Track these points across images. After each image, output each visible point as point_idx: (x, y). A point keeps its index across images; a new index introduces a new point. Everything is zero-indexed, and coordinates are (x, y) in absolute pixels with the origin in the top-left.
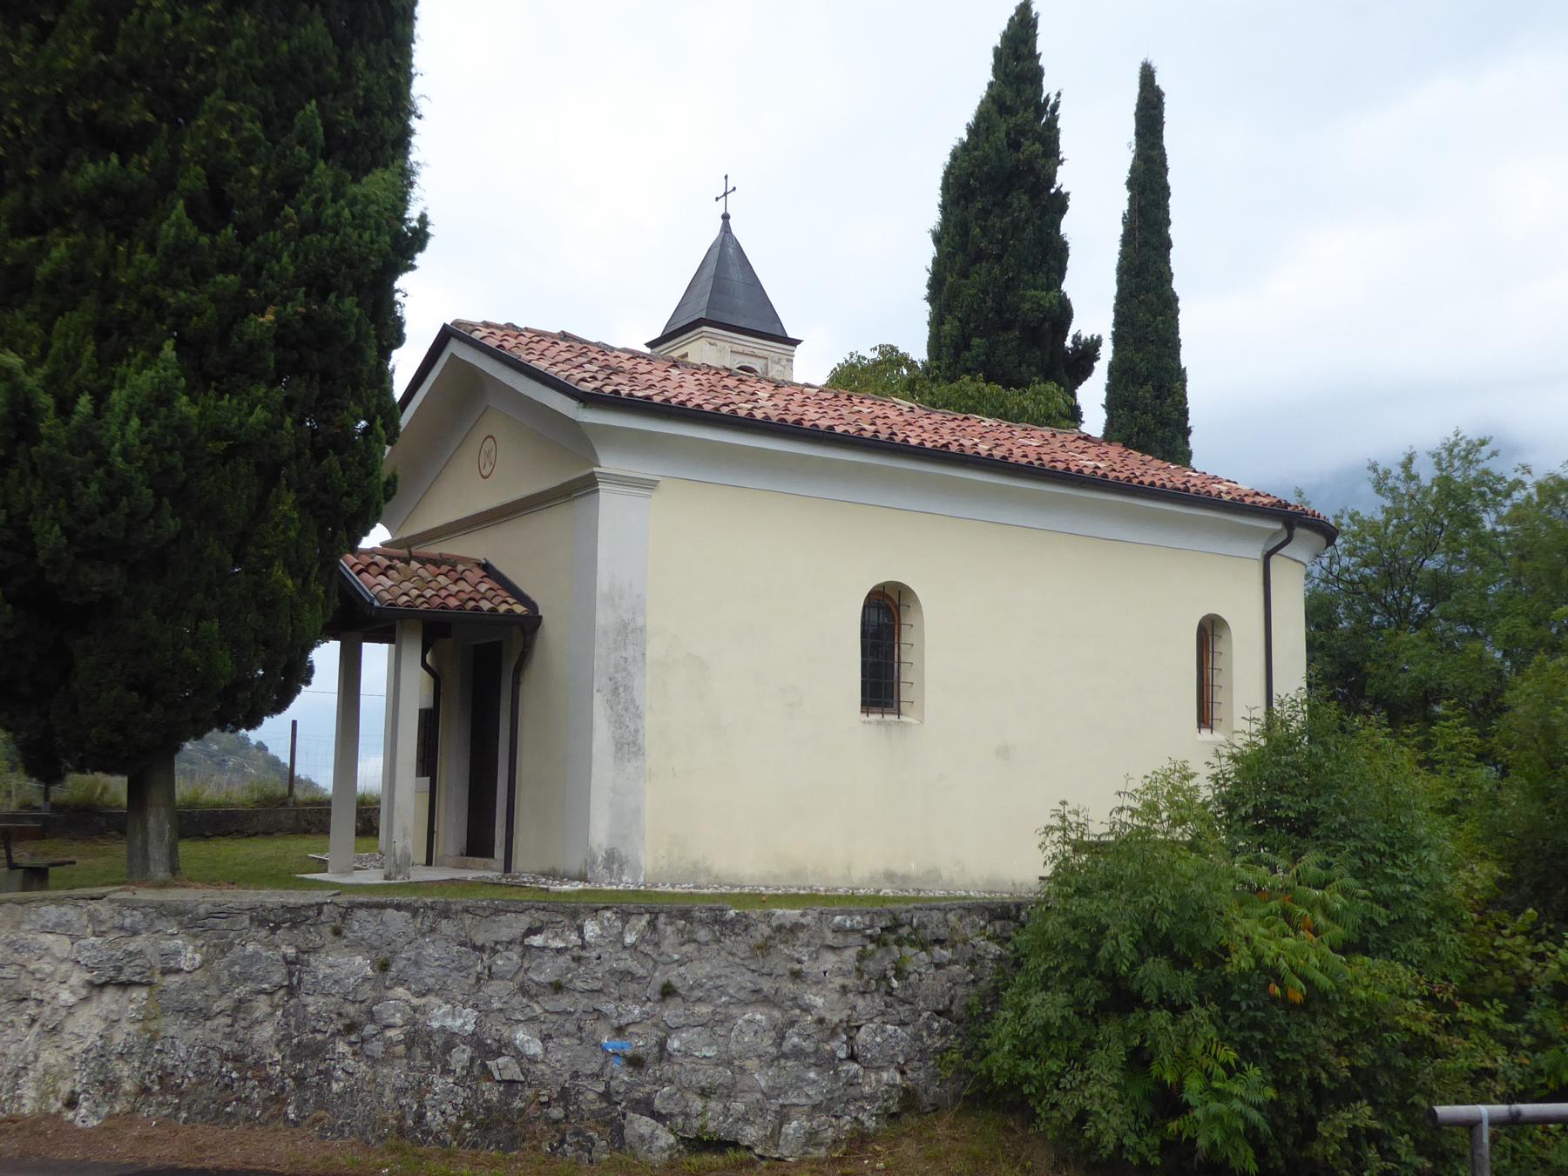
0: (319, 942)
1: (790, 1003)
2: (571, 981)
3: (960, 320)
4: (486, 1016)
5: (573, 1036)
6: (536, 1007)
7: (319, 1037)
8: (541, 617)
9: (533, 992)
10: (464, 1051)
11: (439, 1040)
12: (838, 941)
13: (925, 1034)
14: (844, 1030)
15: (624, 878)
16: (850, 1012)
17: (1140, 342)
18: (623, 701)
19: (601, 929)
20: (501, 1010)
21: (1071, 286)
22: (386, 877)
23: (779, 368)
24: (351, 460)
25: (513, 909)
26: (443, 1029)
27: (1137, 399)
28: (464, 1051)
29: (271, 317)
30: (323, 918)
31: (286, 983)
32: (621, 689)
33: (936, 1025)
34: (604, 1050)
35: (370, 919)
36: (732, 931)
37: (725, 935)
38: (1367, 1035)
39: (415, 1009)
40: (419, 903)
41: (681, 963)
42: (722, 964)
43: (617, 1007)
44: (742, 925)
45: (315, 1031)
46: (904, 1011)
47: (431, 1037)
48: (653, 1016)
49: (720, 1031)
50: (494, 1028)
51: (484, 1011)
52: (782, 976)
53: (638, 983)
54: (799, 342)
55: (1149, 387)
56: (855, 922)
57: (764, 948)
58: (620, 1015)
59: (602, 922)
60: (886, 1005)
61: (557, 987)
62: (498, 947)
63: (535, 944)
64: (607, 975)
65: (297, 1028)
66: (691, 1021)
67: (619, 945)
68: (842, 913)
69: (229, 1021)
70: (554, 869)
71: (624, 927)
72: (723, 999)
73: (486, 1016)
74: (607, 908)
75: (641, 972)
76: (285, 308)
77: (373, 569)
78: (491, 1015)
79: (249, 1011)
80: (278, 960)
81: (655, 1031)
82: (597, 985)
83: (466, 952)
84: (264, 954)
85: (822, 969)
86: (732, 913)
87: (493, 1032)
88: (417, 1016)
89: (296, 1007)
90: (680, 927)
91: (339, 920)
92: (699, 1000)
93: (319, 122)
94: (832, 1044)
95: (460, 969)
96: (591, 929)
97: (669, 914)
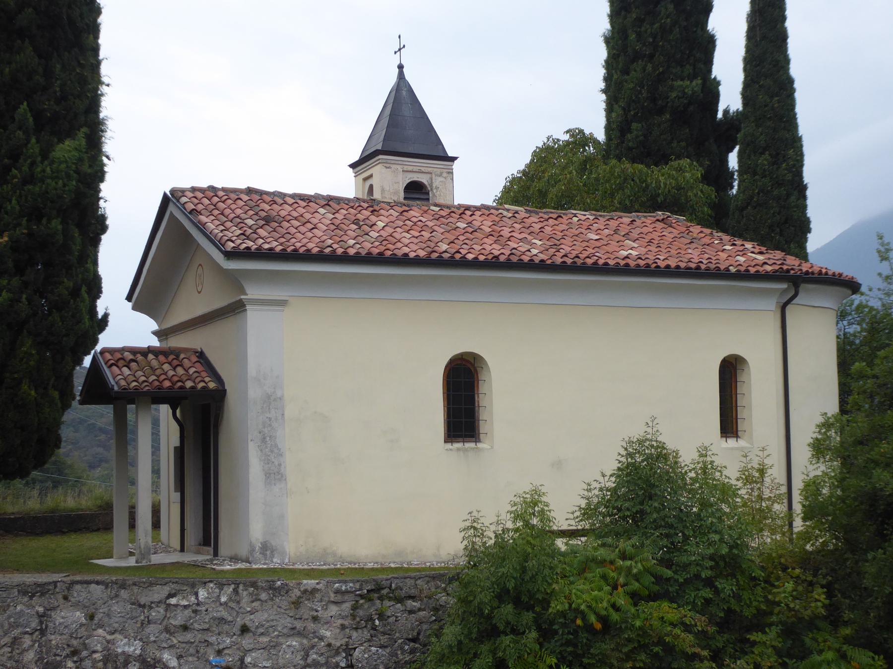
0: (56, 604)
1: (312, 635)
2: (192, 624)
3: (624, 109)
4: (147, 645)
5: (194, 655)
6: (174, 639)
7: (58, 658)
8: (226, 390)
9: (172, 631)
10: (135, 665)
11: (121, 659)
12: (339, 598)
13: (399, 652)
14: (344, 650)
15: (275, 560)
16: (347, 640)
17: (760, 119)
18: (269, 446)
19: (208, 594)
20: (155, 642)
21: (717, 71)
22: (137, 562)
23: (442, 179)
24: (66, 314)
25: (159, 583)
26: (124, 653)
27: (757, 166)
28: (135, 665)
29: (6, 239)
30: (57, 590)
31: (39, 628)
32: (268, 438)
33: (406, 647)
34: (210, 663)
35: (83, 590)
36: (279, 593)
37: (276, 596)
38: (643, 647)
39: (108, 642)
40: (109, 581)
41: (251, 613)
42: (274, 613)
43: (217, 639)
44: (285, 590)
45: (56, 655)
46: (384, 639)
47: (117, 657)
48: (237, 644)
49: (273, 652)
50: (151, 652)
51: (145, 643)
52: (307, 619)
53: (229, 625)
54: (456, 158)
55: (767, 155)
56: (348, 587)
57: (297, 604)
58: (219, 643)
59: (208, 590)
60: (371, 636)
61: (185, 628)
62: (153, 605)
63: (172, 603)
64: (212, 621)
65: (47, 653)
66: (257, 646)
67: (218, 603)
68: (339, 582)
69: (9, 649)
70: (236, 555)
71: (220, 592)
72: (276, 633)
73: (147, 645)
74: (211, 582)
75: (230, 619)
76: (15, 231)
77: (121, 363)
78: (150, 645)
79: (20, 644)
80: (33, 615)
81: (238, 652)
82: (206, 626)
83: (135, 608)
84: (26, 611)
85: (330, 615)
86: (279, 583)
87: (151, 654)
88: (110, 645)
89: (46, 641)
90: (251, 592)
91: (66, 591)
92: (262, 634)
93: (29, 114)
94: (337, 658)
95: (132, 618)
96: (202, 594)
97: (244, 584)
